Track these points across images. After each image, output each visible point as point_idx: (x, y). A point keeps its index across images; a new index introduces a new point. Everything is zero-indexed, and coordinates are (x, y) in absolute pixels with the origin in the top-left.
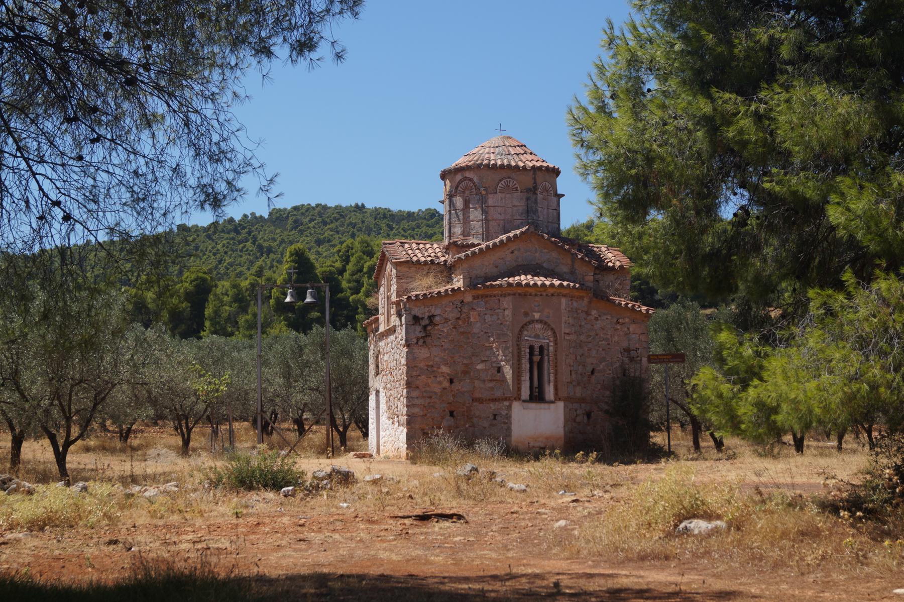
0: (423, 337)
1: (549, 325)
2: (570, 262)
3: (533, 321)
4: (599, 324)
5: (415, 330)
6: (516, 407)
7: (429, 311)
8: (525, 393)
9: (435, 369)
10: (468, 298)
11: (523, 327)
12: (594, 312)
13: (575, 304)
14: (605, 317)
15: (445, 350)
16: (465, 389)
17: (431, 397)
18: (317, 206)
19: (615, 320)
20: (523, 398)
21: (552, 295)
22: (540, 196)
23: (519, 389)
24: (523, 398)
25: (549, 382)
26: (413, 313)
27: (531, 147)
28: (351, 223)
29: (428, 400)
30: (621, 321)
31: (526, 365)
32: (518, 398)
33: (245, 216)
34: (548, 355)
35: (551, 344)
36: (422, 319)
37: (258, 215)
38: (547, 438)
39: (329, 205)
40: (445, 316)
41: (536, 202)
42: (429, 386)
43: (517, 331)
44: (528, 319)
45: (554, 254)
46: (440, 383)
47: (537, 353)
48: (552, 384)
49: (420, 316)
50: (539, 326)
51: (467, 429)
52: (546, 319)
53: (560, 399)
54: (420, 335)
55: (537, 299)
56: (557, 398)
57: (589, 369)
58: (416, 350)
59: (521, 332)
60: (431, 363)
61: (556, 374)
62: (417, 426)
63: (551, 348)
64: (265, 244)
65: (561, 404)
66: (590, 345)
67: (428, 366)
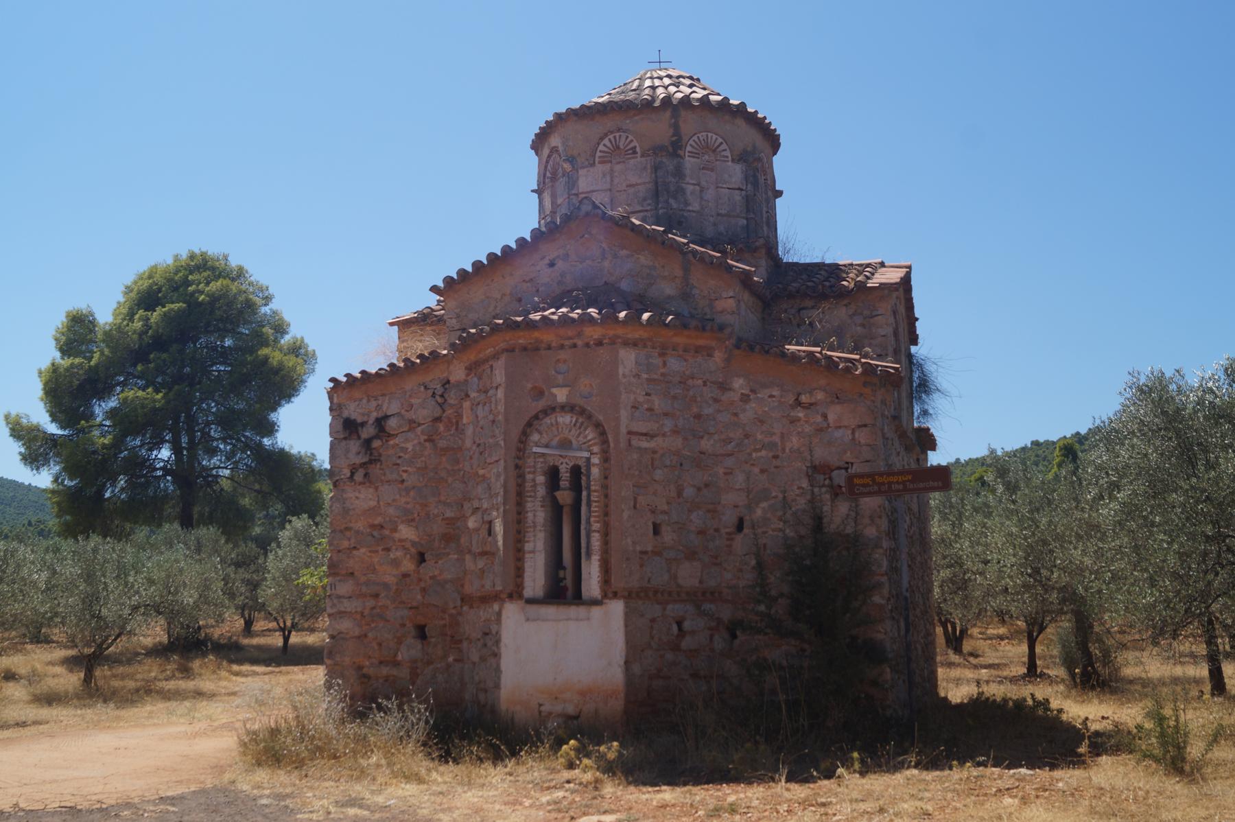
0: (363, 465)
1: (590, 417)
2: (678, 272)
3: (553, 409)
4: (749, 412)
5: (347, 451)
6: (512, 613)
7: (379, 407)
8: (535, 579)
9: (387, 532)
10: (458, 373)
11: (529, 424)
12: (738, 383)
14: (767, 392)
15: (407, 490)
16: (448, 576)
17: (376, 596)
19: (791, 399)
20: (528, 592)
21: (599, 343)
22: (689, 162)
23: (519, 572)
24: (528, 592)
25: (589, 555)
26: (346, 414)
27: (704, 82)
29: (371, 603)
30: (803, 398)
31: (537, 514)
32: (516, 593)
34: (588, 488)
35: (595, 460)
36: (363, 424)
38: (583, 693)
40: (411, 415)
41: (679, 172)
42: (374, 571)
44: (542, 404)
45: (644, 259)
46: (396, 563)
47: (564, 483)
48: (595, 558)
49: (359, 420)
50: (566, 419)
51: (449, 666)
52: (580, 402)
53: (615, 595)
54: (359, 460)
55: (563, 355)
56: (609, 592)
57: (729, 518)
58: (350, 493)
59: (525, 434)
60: (378, 520)
61: (606, 534)
62: (347, 660)
63: (595, 471)
65: (617, 608)
66: (729, 462)
67: (373, 526)
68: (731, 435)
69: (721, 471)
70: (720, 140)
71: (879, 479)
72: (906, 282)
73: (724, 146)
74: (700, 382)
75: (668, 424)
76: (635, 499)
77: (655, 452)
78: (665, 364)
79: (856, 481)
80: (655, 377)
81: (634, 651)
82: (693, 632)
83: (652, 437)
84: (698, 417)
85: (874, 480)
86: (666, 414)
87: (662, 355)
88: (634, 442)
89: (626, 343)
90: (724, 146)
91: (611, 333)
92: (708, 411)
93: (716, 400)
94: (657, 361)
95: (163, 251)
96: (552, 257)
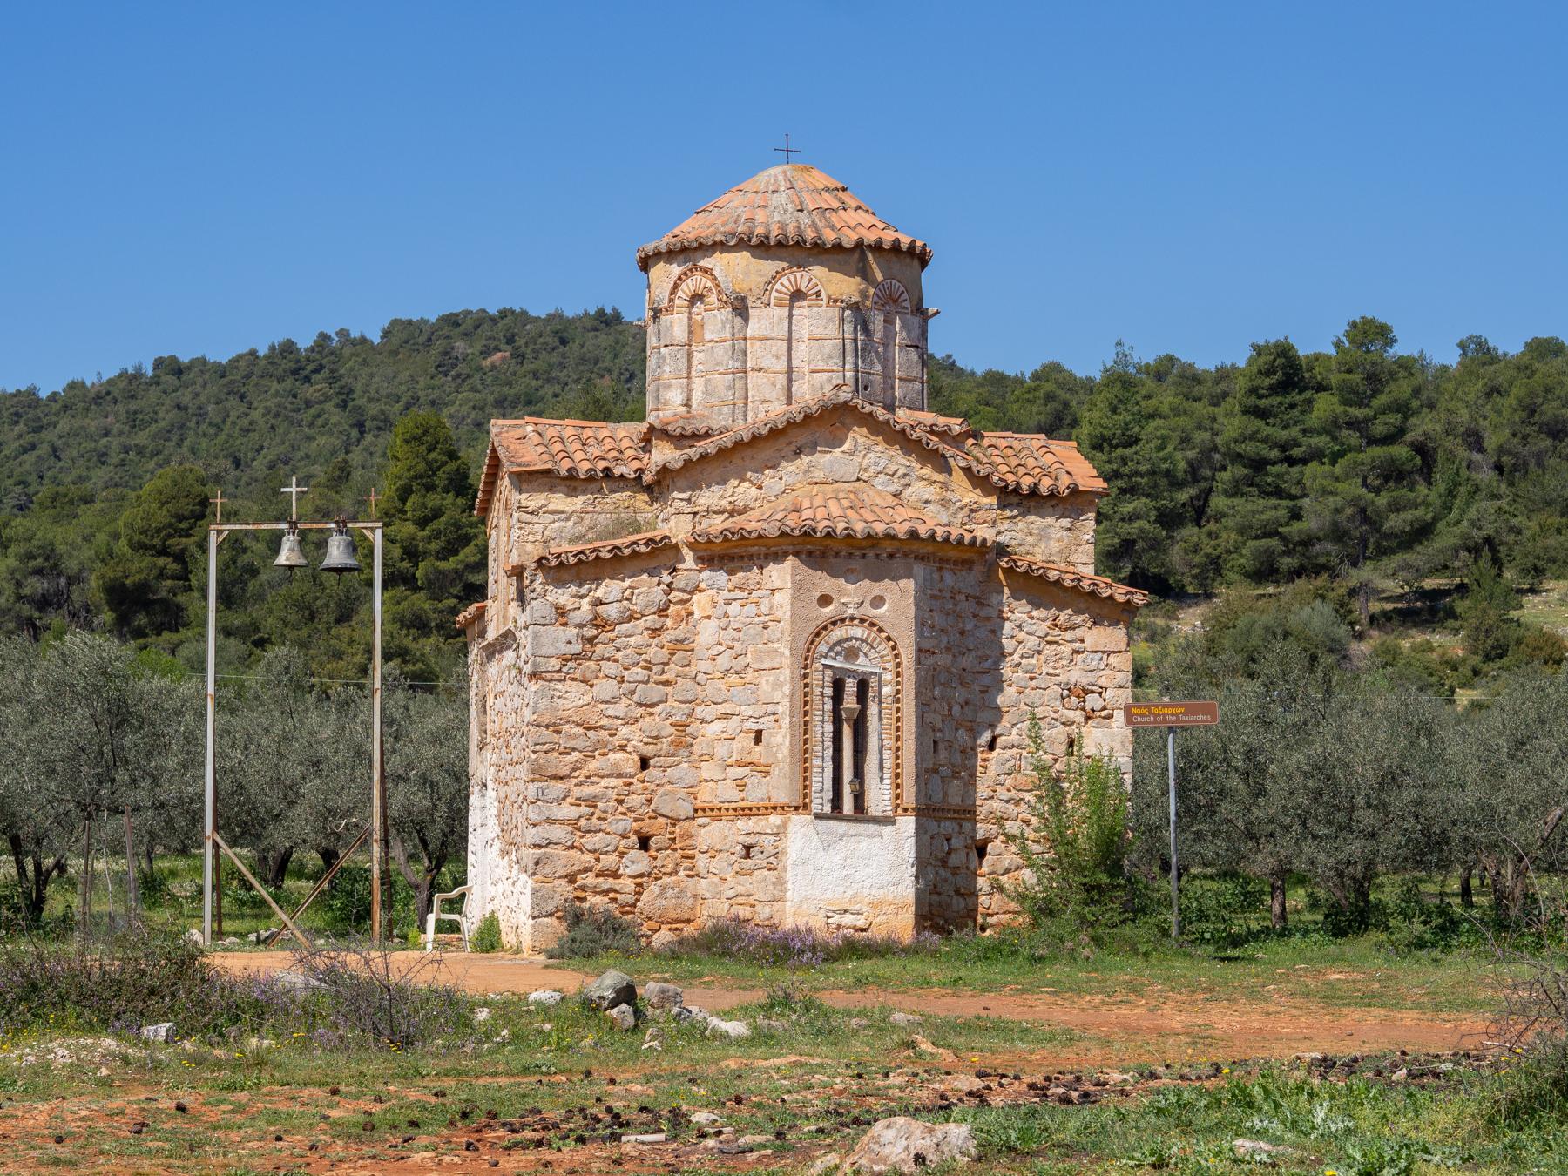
13: (949, 579)
18: (504, 313)
20: (816, 807)
24: (816, 807)
28: (583, 360)
32: (802, 807)
33: (324, 337)
35: (888, 677)
37: (355, 333)
39: (533, 313)
43: (802, 645)
64: (374, 409)
65: (908, 824)
73: (905, 296)
87: (940, 569)
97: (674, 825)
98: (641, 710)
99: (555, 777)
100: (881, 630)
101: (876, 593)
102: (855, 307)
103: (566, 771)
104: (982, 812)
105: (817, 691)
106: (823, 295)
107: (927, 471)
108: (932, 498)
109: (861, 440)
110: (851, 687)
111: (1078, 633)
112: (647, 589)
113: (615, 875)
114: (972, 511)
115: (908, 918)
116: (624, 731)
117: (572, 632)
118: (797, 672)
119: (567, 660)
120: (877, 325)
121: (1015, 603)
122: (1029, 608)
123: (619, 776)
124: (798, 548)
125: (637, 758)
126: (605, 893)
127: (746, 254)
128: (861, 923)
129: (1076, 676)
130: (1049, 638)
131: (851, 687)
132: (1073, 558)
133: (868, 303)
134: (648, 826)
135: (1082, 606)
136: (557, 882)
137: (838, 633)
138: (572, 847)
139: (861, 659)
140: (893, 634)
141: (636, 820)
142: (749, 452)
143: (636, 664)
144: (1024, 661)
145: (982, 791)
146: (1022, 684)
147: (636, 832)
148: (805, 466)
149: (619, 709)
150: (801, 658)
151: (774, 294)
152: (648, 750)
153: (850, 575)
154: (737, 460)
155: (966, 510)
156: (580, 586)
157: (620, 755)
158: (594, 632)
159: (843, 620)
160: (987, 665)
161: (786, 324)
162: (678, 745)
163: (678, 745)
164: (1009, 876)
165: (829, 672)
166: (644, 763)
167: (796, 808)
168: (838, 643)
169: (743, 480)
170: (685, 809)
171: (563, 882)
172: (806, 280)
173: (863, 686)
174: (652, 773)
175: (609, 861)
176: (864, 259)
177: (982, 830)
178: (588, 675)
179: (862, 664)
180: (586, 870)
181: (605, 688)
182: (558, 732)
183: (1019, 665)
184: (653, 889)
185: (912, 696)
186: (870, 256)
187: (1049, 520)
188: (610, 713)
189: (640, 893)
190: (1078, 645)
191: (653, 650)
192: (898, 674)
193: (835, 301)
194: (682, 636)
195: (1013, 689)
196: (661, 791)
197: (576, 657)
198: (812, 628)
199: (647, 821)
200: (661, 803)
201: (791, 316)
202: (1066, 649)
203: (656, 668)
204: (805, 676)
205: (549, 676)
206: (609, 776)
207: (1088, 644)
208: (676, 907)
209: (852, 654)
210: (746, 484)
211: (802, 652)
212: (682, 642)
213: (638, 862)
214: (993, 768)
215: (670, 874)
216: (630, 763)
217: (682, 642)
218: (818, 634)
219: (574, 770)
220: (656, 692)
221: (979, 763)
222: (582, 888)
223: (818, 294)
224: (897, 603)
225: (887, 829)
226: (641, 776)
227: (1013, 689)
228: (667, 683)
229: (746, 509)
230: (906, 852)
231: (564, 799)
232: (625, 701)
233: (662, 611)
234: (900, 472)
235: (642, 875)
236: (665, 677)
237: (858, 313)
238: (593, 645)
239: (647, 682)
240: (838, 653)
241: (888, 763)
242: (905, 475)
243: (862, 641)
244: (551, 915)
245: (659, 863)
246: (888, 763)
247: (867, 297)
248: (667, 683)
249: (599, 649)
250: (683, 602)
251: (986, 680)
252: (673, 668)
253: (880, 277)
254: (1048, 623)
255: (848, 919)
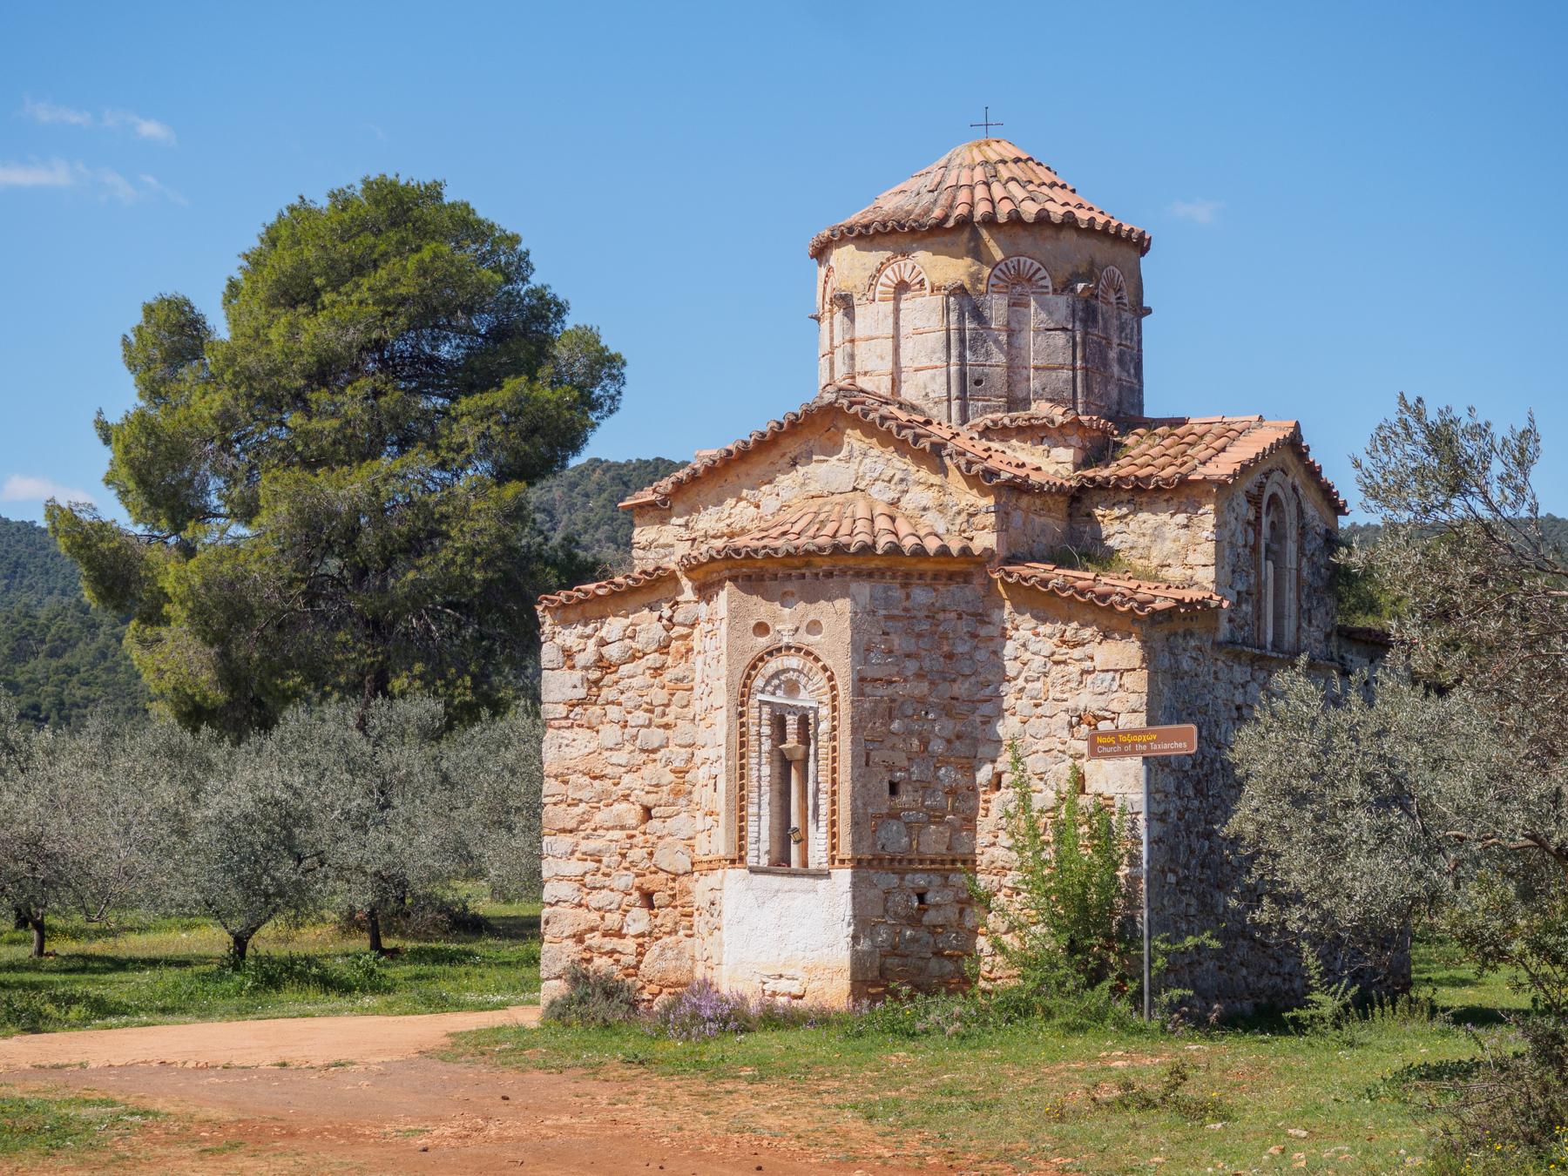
20: (751, 860)
21: (829, 575)
32: (737, 860)
43: (738, 680)
44: (763, 642)
63: (824, 726)
65: (843, 876)
68: (990, 677)
69: (978, 719)
70: (1037, 265)
71: (1122, 738)
72: (1294, 444)
73: (1043, 273)
74: (953, 615)
75: (911, 666)
76: (868, 755)
77: (893, 701)
78: (908, 597)
79: (1100, 740)
80: (896, 612)
81: (862, 924)
82: (938, 906)
83: (890, 682)
84: (950, 656)
85: (1117, 739)
86: (908, 656)
87: (905, 586)
88: (868, 690)
89: (858, 574)
90: (1043, 273)
91: (841, 565)
92: (961, 648)
93: (974, 636)
94: (898, 593)
95: (329, 169)
96: (793, 455)
97: (674, 880)
98: (644, 756)
99: (564, 831)
100: (817, 659)
101: (812, 617)
102: (960, 291)
103: (572, 824)
104: (983, 861)
105: (753, 730)
106: (927, 284)
107: (924, 474)
108: (930, 504)
109: (856, 445)
110: (792, 722)
111: (1088, 649)
112: (648, 625)
113: (619, 934)
114: (971, 515)
115: (843, 984)
116: (627, 779)
117: (577, 675)
118: (733, 711)
119: (574, 706)
120: (997, 308)
121: (1019, 619)
122: (1033, 623)
123: (623, 828)
124: (734, 572)
125: (639, 808)
126: (611, 953)
127: (851, 247)
128: (796, 990)
129: (1085, 700)
130: (1056, 658)
131: (792, 722)
132: (1191, 559)
133: (982, 287)
134: (650, 882)
135: (1089, 617)
136: (566, 942)
137: (774, 664)
138: (580, 905)
139: (803, 694)
140: (829, 663)
141: (637, 876)
142: (743, 468)
143: (638, 707)
144: (1029, 686)
145: (983, 838)
146: (1026, 712)
147: (638, 888)
148: (800, 480)
149: (621, 757)
150: (736, 694)
151: (879, 288)
152: (650, 800)
153: (785, 599)
154: (731, 478)
155: (964, 515)
156: (586, 625)
157: (625, 805)
158: (597, 674)
159: (779, 650)
160: (988, 691)
161: (891, 320)
162: (677, 793)
163: (677, 793)
164: (1011, 932)
165: (766, 709)
166: (647, 813)
167: (733, 861)
168: (776, 675)
169: (740, 499)
170: (683, 864)
171: (570, 942)
172: (909, 268)
173: (804, 722)
174: (655, 824)
175: (613, 920)
176: (976, 237)
177: (983, 880)
178: (594, 721)
179: (804, 699)
180: (592, 930)
181: (610, 734)
182: (566, 782)
183: (1022, 690)
184: (655, 949)
185: (848, 732)
186: (985, 234)
187: (1165, 517)
188: (614, 760)
189: (641, 954)
190: (1088, 665)
191: (655, 690)
192: (834, 709)
193: (939, 289)
194: (681, 675)
195: (1017, 719)
196: (661, 843)
197: (581, 702)
198: (748, 659)
199: (649, 876)
200: (663, 859)
201: (897, 311)
202: (1074, 669)
203: (658, 710)
204: (741, 715)
205: (556, 723)
206: (613, 828)
207: (1098, 663)
208: (676, 969)
209: (792, 688)
210: (743, 504)
211: (738, 688)
212: (681, 680)
213: (639, 920)
214: (995, 812)
215: (669, 933)
216: (629, 813)
217: (681, 680)
218: (754, 667)
219: (581, 822)
220: (655, 736)
221: (981, 804)
222: (589, 949)
223: (921, 283)
224: (829, 627)
225: (822, 883)
226: (642, 828)
227: (1017, 719)
228: (667, 726)
229: (743, 532)
230: (842, 909)
231: (573, 853)
232: (629, 747)
233: (663, 648)
234: (896, 479)
235: (642, 935)
236: (665, 720)
237: (965, 300)
238: (600, 689)
239: (649, 726)
240: (777, 687)
241: (824, 808)
242: (902, 480)
243: (800, 672)
244: (559, 977)
245: (658, 921)
246: (824, 808)
247: (980, 281)
248: (667, 726)
249: (604, 691)
250: (685, 637)
251: (986, 709)
252: (673, 710)
253: (998, 255)
254: (1055, 640)
255: (783, 986)
